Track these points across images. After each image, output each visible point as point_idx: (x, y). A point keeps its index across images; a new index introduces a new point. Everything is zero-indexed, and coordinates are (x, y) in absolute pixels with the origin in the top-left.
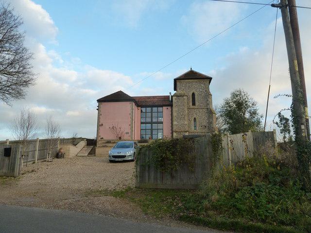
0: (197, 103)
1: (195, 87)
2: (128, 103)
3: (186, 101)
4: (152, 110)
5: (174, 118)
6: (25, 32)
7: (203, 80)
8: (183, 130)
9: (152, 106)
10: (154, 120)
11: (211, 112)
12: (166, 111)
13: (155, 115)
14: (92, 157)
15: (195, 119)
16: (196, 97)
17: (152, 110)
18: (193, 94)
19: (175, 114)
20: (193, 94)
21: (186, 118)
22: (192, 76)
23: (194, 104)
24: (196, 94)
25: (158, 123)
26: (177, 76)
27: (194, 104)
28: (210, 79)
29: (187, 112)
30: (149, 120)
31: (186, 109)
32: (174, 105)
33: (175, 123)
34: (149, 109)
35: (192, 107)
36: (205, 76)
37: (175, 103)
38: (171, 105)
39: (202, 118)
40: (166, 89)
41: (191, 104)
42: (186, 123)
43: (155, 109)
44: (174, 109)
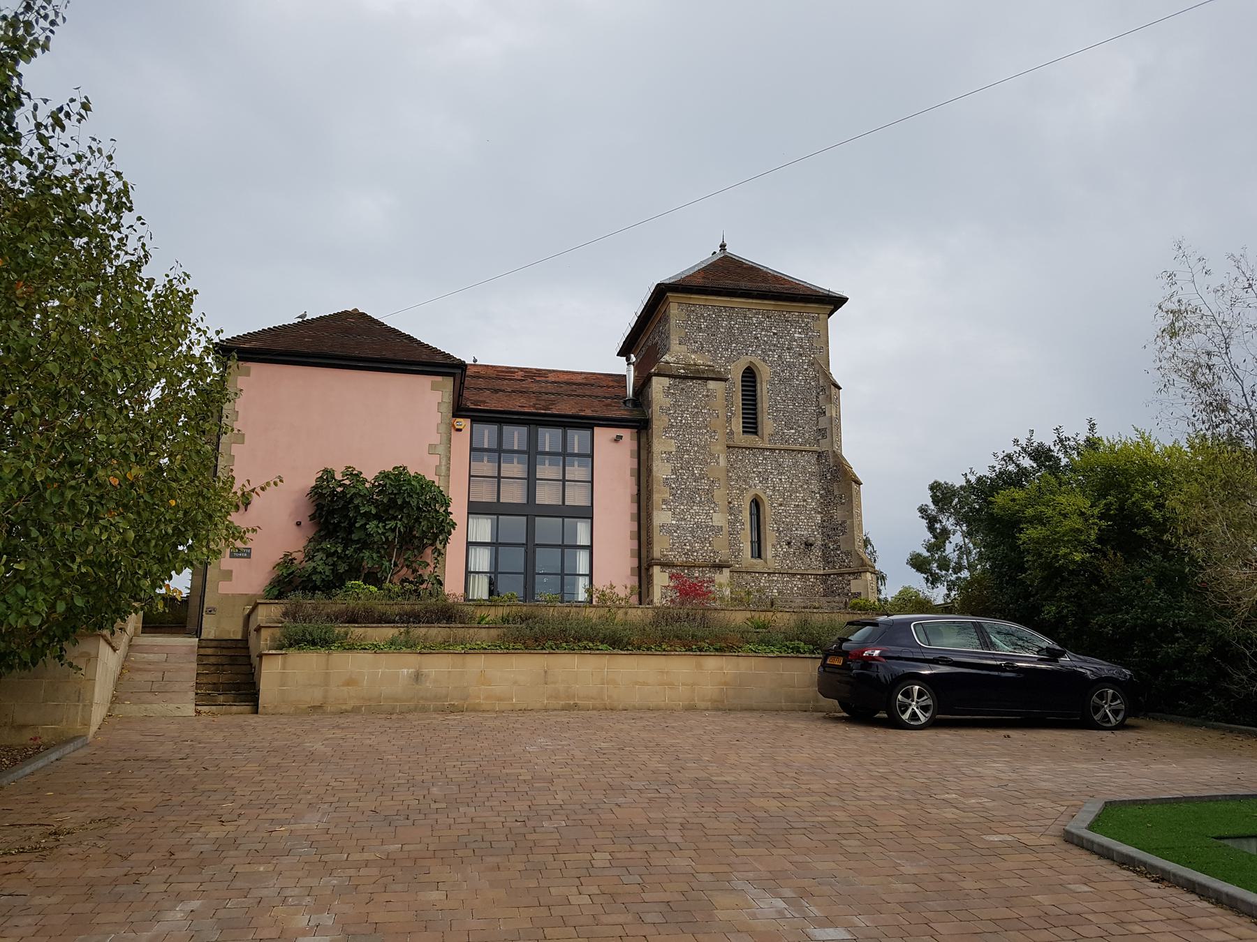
0: (768, 424)
1: (755, 336)
2: (425, 382)
3: (719, 401)
4: (532, 440)
5: (660, 494)
6: (1092, 427)
7: (768, 305)
9: (534, 421)
10: (546, 496)
11: (838, 482)
12: (612, 451)
13: (546, 470)
14: (615, 445)
15: (756, 503)
16: (764, 389)
17: (532, 440)
18: (750, 376)
19: (661, 470)
20: (750, 376)
21: (719, 494)
22: (729, 281)
23: (751, 426)
24: (765, 372)
26: (670, 271)
27: (751, 426)
28: (836, 302)
29: (722, 462)
30: (514, 494)
31: (718, 448)
32: (658, 423)
33: (661, 517)
34: (516, 436)
35: (741, 439)
36: (778, 278)
38: (641, 426)
40: (580, 335)
42: (719, 519)
43: (548, 438)
44: (662, 444)
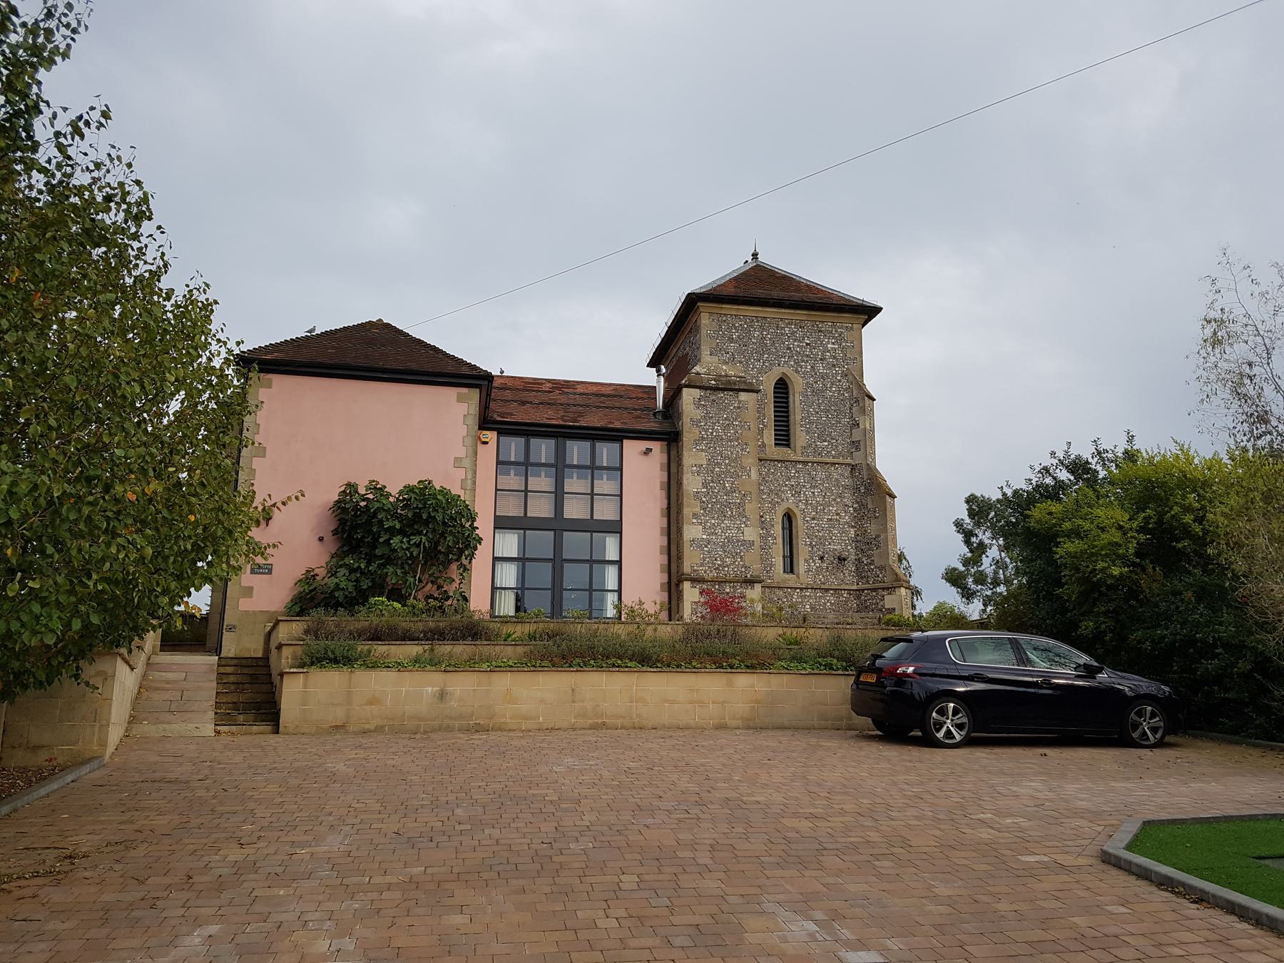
0: (800, 437)
1: (786, 346)
2: (451, 393)
3: (750, 414)
4: (560, 453)
5: (690, 508)
6: (1131, 439)
8: (731, 572)
9: (561, 433)
10: (574, 510)
12: (641, 465)
13: (574, 484)
15: (789, 517)
16: (796, 401)
17: (560, 453)
18: (782, 387)
19: (692, 484)
20: (782, 387)
21: (751, 508)
23: (783, 438)
24: (798, 384)
25: (593, 527)
26: (701, 280)
27: (783, 438)
29: (754, 475)
30: (541, 508)
31: (750, 461)
32: (688, 436)
33: (692, 532)
34: (544, 449)
35: (774, 452)
37: (696, 423)
38: (671, 438)
39: (828, 521)
40: (611, 347)
41: (769, 437)
42: (751, 534)
43: (577, 451)
44: (692, 457)
